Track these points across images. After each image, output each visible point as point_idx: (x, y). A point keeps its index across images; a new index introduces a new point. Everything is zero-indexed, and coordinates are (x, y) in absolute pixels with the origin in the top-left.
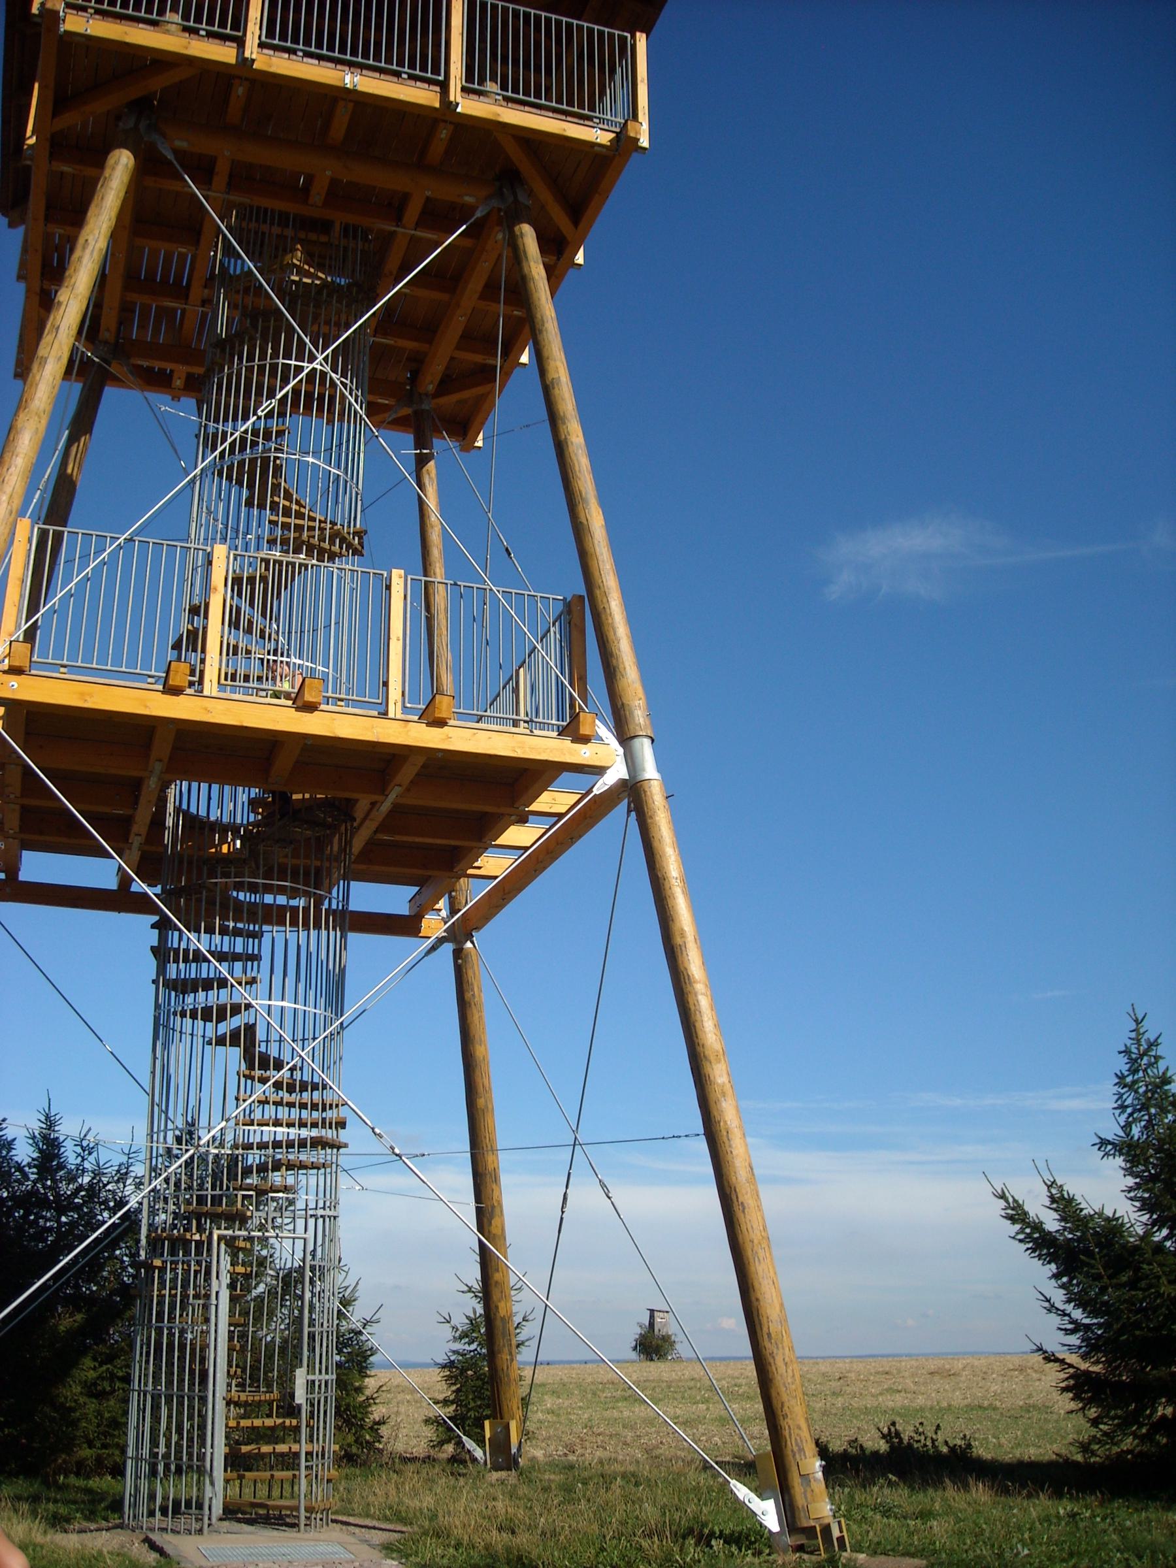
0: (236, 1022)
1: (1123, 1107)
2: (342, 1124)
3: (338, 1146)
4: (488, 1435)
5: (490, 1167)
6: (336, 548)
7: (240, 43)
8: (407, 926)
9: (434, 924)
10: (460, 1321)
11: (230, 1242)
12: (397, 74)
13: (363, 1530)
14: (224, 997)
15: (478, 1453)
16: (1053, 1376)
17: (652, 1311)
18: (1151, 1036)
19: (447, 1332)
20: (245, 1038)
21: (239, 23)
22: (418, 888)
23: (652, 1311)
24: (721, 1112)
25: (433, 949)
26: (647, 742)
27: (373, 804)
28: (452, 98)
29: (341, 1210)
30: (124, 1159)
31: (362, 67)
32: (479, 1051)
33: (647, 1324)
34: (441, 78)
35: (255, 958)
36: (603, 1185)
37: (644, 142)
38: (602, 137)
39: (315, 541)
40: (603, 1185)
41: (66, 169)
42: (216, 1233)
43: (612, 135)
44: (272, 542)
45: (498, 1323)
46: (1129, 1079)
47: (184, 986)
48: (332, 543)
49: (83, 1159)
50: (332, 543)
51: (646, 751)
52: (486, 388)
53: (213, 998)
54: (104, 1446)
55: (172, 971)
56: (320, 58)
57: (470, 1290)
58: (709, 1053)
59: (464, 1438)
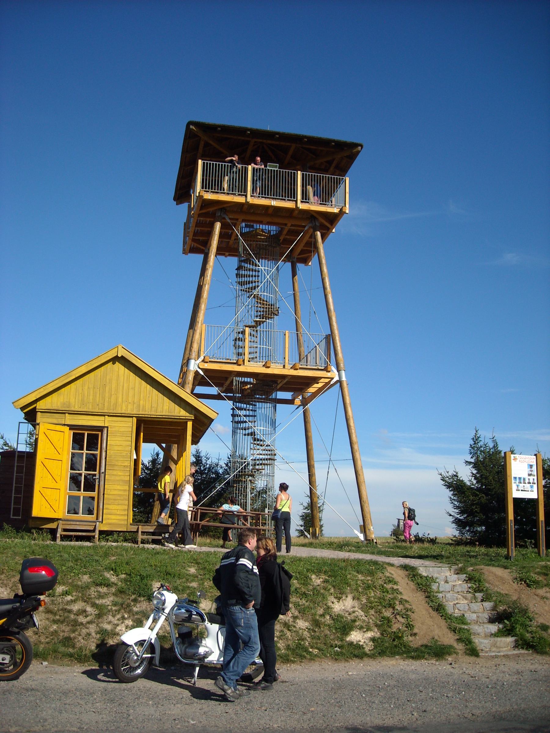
0: (250, 431)
1: (471, 453)
2: (275, 455)
3: (274, 460)
4: (311, 531)
5: (312, 464)
6: (272, 316)
7: (246, 196)
8: (291, 402)
9: (298, 401)
10: (306, 505)
11: (250, 481)
12: (285, 200)
13: (302, 340)
14: (247, 425)
15: (309, 536)
16: (451, 519)
17: (399, 520)
18: (478, 435)
19: (302, 507)
20: (253, 434)
21: (246, 191)
22: (293, 393)
23: (399, 520)
24: (355, 455)
25: (298, 408)
26: (343, 371)
27: (282, 381)
28: (298, 206)
29: (275, 474)
30: (217, 461)
31: (275, 199)
32: (309, 434)
33: (397, 525)
34: (295, 199)
35: (255, 416)
36: (335, 469)
37: (347, 211)
38: (336, 210)
39: (267, 316)
40: (335, 469)
41: (202, 219)
42: (248, 479)
43: (339, 210)
44: (257, 316)
45: (314, 503)
46: (473, 446)
47: (238, 422)
48: (271, 315)
49: (207, 461)
50: (271, 315)
51: (343, 373)
52: (310, 254)
53: (244, 425)
54: (215, 532)
55: (237, 419)
56: (265, 198)
57: (308, 496)
58: (354, 443)
59: (305, 532)
